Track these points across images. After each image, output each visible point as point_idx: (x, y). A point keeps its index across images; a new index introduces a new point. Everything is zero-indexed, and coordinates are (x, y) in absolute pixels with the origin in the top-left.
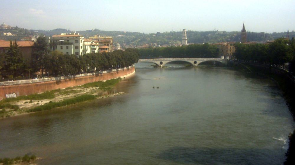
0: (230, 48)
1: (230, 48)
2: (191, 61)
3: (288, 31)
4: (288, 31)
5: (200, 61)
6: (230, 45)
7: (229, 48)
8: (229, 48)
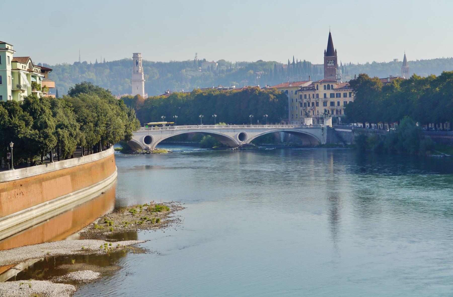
0: (325, 95)
1: (325, 95)
2: (231, 132)
3: (97, 62)
4: (97, 62)
5: (253, 132)
6: (325, 89)
7: (321, 96)
8: (321, 96)
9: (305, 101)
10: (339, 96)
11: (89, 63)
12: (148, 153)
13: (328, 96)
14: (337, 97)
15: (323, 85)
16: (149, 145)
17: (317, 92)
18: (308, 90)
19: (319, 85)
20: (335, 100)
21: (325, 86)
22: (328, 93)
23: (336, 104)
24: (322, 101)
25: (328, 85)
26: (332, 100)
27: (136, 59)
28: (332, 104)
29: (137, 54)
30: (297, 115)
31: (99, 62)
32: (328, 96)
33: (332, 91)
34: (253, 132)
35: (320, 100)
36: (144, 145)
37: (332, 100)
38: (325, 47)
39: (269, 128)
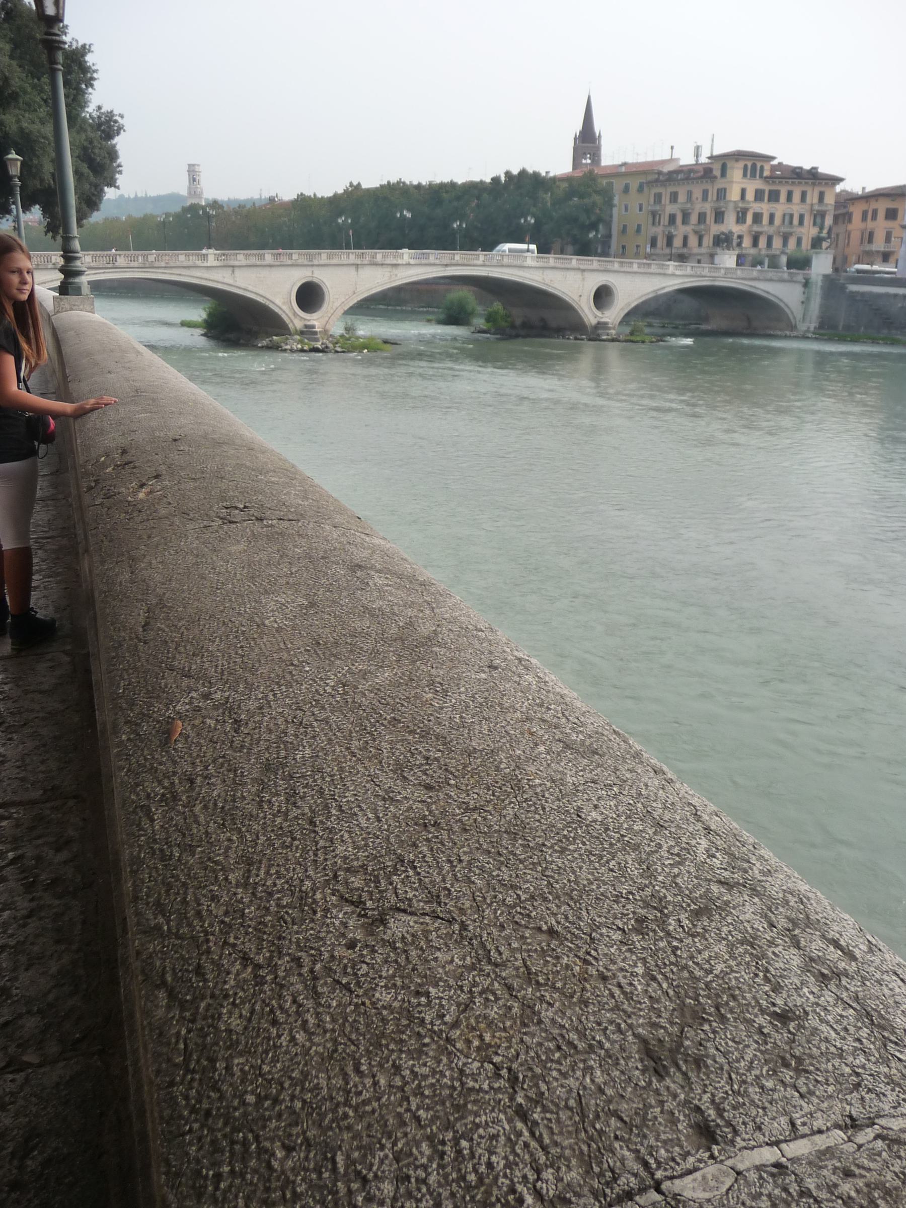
0: (743, 192)
1: (743, 192)
2: (570, 280)
6: (745, 175)
9: (670, 209)
10: (774, 197)
11: (126, 196)
12: (314, 345)
13: (750, 196)
14: (769, 200)
15: (741, 164)
16: (315, 316)
17: (720, 184)
18: (687, 179)
19: (729, 164)
20: (764, 208)
21: (746, 167)
22: (752, 186)
23: (765, 220)
24: (736, 207)
25: (754, 166)
26: (757, 207)
27: (192, 174)
28: (757, 218)
29: (194, 165)
30: (638, 246)
31: (139, 195)
32: (750, 196)
33: (758, 184)
34: (637, 284)
35: (731, 205)
36: (295, 314)
37: (757, 207)
38: (578, 126)
39: (678, 272)
